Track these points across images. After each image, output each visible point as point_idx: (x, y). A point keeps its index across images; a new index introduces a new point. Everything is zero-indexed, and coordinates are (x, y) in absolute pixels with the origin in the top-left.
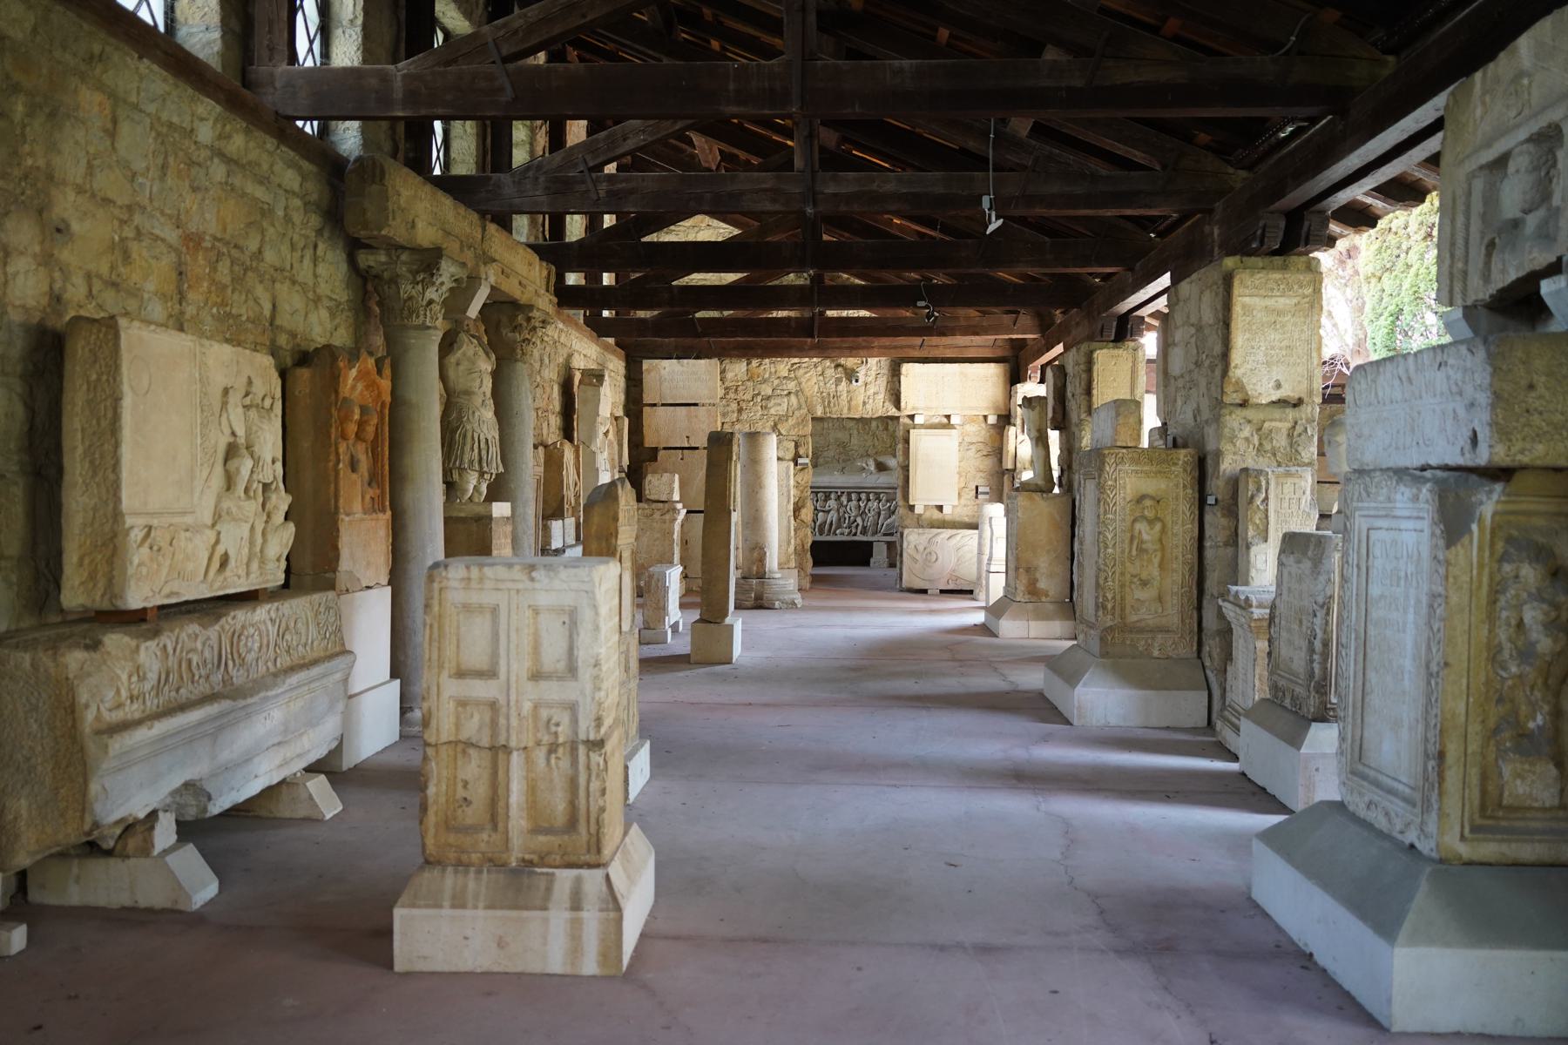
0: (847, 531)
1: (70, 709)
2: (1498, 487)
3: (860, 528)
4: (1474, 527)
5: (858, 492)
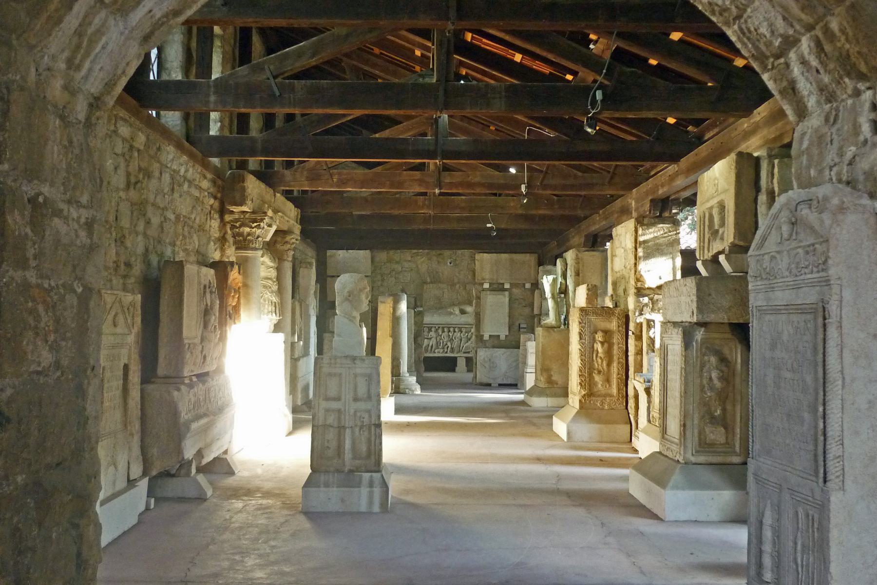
0: (442, 350)
1: (175, 413)
2: (703, 329)
3: (449, 349)
4: (694, 343)
5: (448, 327)
